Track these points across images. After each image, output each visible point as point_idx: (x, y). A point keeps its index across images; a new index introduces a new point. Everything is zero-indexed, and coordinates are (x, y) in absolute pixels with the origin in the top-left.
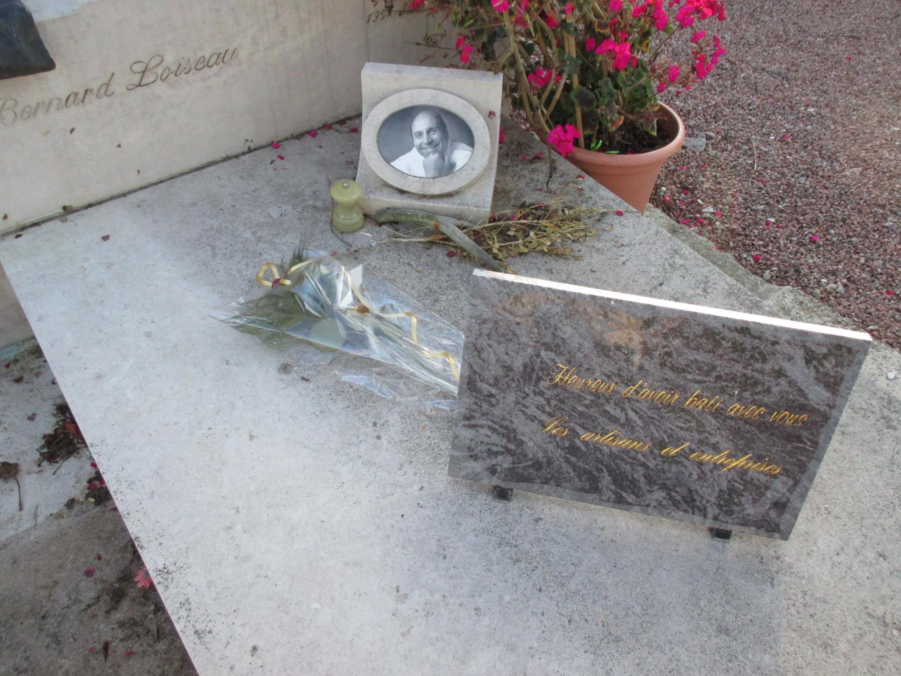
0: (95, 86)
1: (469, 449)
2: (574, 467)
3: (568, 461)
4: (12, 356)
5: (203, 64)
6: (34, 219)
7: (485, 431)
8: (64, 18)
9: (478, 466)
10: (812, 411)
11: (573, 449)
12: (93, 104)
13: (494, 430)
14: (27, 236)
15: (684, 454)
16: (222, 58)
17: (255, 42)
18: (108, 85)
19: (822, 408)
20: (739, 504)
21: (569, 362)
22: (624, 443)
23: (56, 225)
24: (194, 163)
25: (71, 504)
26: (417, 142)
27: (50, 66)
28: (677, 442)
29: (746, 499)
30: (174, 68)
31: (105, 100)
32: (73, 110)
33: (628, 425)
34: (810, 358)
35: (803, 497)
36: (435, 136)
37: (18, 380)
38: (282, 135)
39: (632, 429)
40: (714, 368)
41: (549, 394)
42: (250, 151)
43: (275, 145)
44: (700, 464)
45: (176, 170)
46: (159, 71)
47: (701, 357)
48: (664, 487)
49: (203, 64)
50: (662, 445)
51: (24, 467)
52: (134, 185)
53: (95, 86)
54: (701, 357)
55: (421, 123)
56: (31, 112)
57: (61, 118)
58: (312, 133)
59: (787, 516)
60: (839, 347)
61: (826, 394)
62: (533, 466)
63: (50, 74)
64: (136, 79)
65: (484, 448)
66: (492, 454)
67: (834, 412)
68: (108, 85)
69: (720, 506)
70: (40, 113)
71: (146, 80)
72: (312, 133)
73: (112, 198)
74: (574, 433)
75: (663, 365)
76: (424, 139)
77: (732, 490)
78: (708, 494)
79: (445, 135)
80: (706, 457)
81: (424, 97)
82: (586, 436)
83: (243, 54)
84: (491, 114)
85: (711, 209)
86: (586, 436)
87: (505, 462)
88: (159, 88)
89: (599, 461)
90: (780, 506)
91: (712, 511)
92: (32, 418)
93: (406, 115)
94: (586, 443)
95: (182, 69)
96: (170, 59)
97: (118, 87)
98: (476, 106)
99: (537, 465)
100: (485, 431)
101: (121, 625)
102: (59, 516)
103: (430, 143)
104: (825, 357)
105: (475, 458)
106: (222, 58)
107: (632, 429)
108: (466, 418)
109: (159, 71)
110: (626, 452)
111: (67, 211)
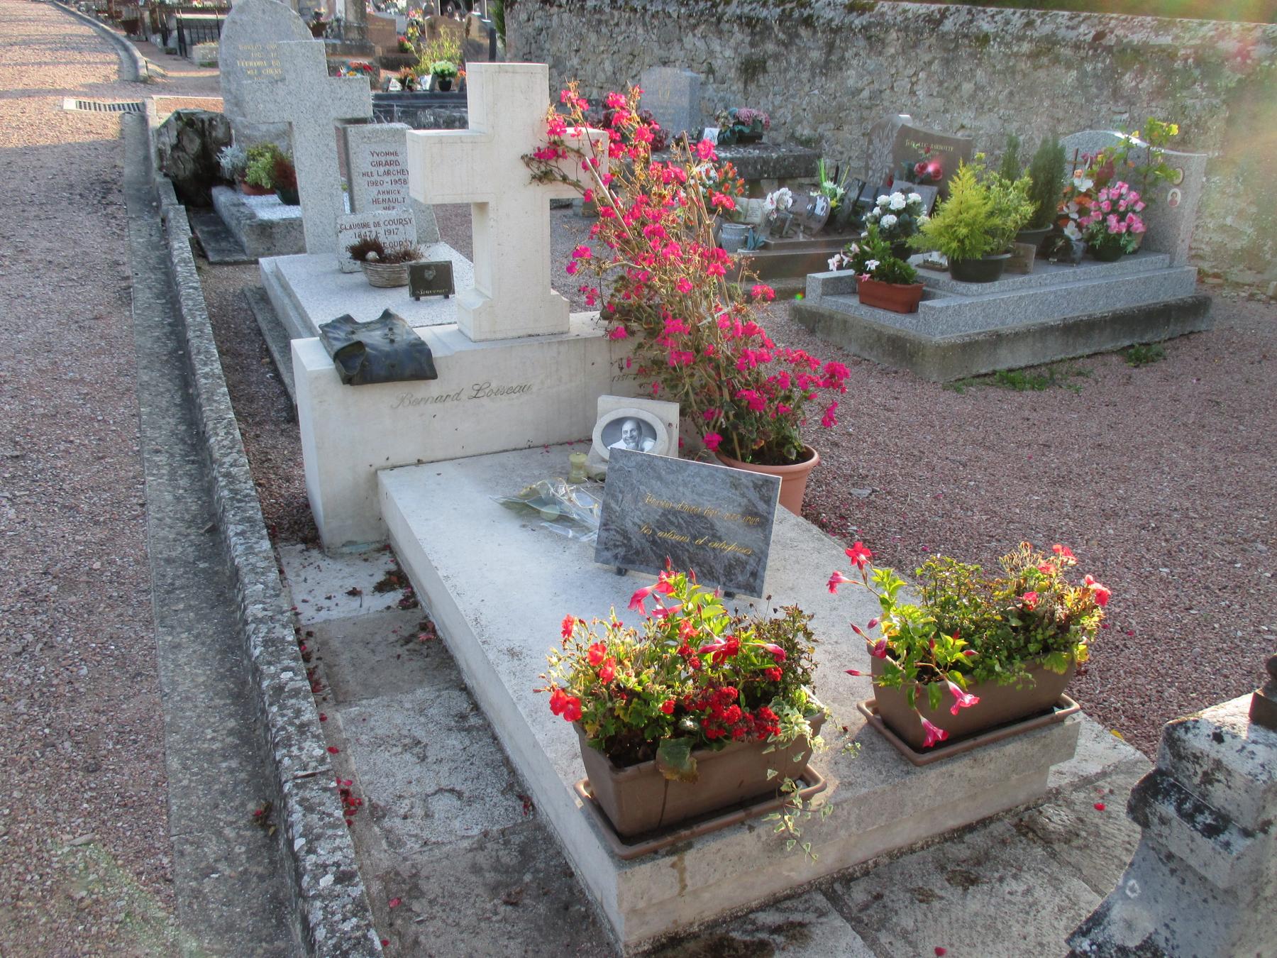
0: (452, 394)
1: (606, 544)
2: (655, 553)
3: (652, 549)
4: (363, 550)
5: (511, 391)
6: (402, 463)
7: (613, 532)
8: (446, 357)
9: (608, 554)
10: (761, 516)
11: (654, 542)
12: (449, 403)
13: (617, 532)
14: (395, 470)
15: (706, 543)
16: (522, 389)
17: (542, 383)
18: (459, 394)
19: (765, 514)
20: (734, 574)
21: (652, 492)
22: (677, 538)
23: (414, 467)
24: (495, 449)
25: (389, 608)
26: (624, 436)
27: (434, 376)
28: (702, 536)
29: (738, 571)
30: (495, 390)
31: (456, 402)
32: (439, 405)
33: (679, 527)
34: (756, 486)
35: (764, 568)
36: (635, 433)
37: (366, 560)
38: (551, 442)
39: (681, 529)
40: (715, 493)
41: (643, 509)
42: (530, 447)
43: (546, 446)
44: (714, 549)
45: (485, 451)
46: (487, 391)
47: (708, 487)
48: (698, 564)
49: (511, 391)
50: (695, 538)
51: (364, 592)
52: (459, 455)
53: (452, 394)
54: (708, 487)
55: (628, 426)
56: (418, 402)
57: (432, 408)
58: (570, 443)
59: (758, 581)
60: (767, 481)
61: (765, 506)
62: (635, 553)
63: (432, 381)
64: (474, 393)
65: (612, 543)
66: (616, 546)
67: (770, 517)
68: (459, 394)
69: (726, 576)
70: (422, 403)
71: (479, 395)
72: (570, 443)
73: (445, 460)
74: (654, 533)
75: (693, 492)
76: (628, 435)
77: (730, 565)
78: (719, 569)
79: (640, 434)
80: (716, 545)
81: (631, 412)
82: (660, 534)
83: (535, 389)
84: (670, 425)
85: (855, 528)
86: (660, 534)
87: (621, 551)
88: (485, 401)
89: (667, 549)
90: (754, 574)
91: (722, 579)
92: (371, 575)
93: (619, 422)
94: (660, 538)
95: (500, 392)
96: (494, 385)
97: (464, 396)
98: (661, 419)
99: (637, 553)
100: (613, 532)
101: (408, 650)
102: (382, 611)
103: (631, 437)
104: (762, 486)
105: (607, 549)
106: (522, 389)
107: (681, 529)
108: (605, 525)
109: (487, 391)
110: (679, 543)
111: (420, 462)
